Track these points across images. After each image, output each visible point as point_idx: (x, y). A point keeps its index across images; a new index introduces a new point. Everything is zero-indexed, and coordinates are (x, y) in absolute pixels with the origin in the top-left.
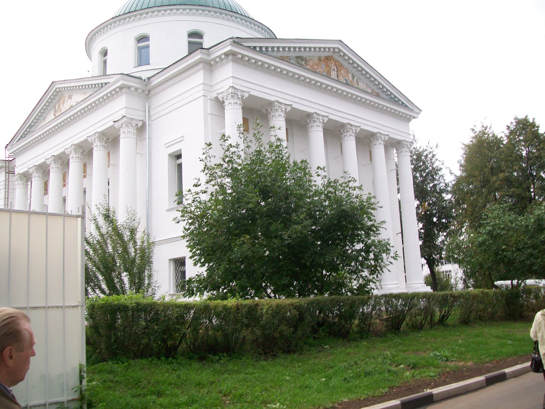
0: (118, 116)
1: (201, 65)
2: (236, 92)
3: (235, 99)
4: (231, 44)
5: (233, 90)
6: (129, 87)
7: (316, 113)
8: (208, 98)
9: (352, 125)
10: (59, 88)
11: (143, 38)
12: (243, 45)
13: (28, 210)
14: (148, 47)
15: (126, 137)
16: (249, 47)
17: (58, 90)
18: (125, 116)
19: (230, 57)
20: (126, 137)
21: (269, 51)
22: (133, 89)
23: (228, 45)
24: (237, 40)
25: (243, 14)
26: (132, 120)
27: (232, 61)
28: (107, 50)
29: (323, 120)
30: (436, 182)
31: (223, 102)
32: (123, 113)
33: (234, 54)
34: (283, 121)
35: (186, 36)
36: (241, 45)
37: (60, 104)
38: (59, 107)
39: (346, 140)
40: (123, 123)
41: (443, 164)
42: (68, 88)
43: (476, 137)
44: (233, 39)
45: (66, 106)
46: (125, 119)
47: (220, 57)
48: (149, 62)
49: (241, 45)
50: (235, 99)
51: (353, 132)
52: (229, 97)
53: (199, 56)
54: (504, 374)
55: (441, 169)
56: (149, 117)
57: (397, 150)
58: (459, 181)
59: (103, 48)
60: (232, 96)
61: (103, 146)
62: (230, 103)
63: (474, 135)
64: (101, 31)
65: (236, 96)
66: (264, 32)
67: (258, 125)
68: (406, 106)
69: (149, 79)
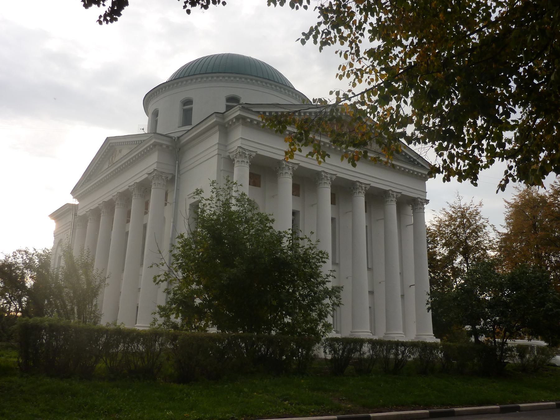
0: (151, 170)
1: (217, 128)
2: (244, 152)
3: (243, 157)
4: (240, 110)
5: (241, 150)
6: (161, 145)
7: (324, 171)
8: (222, 156)
9: (361, 183)
10: (112, 143)
11: (188, 102)
12: (252, 111)
13: (384, 282)
14: (191, 109)
15: (156, 188)
16: (258, 112)
17: (111, 145)
18: (156, 170)
19: (241, 120)
20: (156, 188)
21: (302, 116)
22: (164, 146)
23: (238, 111)
24: (245, 106)
25: (276, 80)
26: (162, 173)
27: (242, 125)
28: (158, 111)
29: (332, 178)
30: (479, 239)
31: (234, 160)
32: (154, 167)
33: (244, 118)
34: (290, 178)
35: (224, 100)
36: (249, 110)
37: (113, 157)
38: (112, 159)
39: (356, 197)
40: (154, 176)
41: (488, 221)
42: (124, 143)
43: (520, 196)
44: (242, 105)
45: (117, 158)
46: (155, 172)
47: (232, 120)
48: (191, 123)
49: (249, 110)
50: (243, 157)
51: (363, 189)
52: (238, 156)
53: (215, 120)
54: (454, 411)
55: (485, 226)
56: (179, 171)
57: (413, 207)
58: (506, 239)
59: (155, 109)
60: (240, 155)
61: (141, 194)
62: (238, 161)
63: (518, 194)
64: (154, 94)
65: (243, 156)
66: (297, 97)
67: (229, 181)
68: (422, 166)
69: (178, 138)
